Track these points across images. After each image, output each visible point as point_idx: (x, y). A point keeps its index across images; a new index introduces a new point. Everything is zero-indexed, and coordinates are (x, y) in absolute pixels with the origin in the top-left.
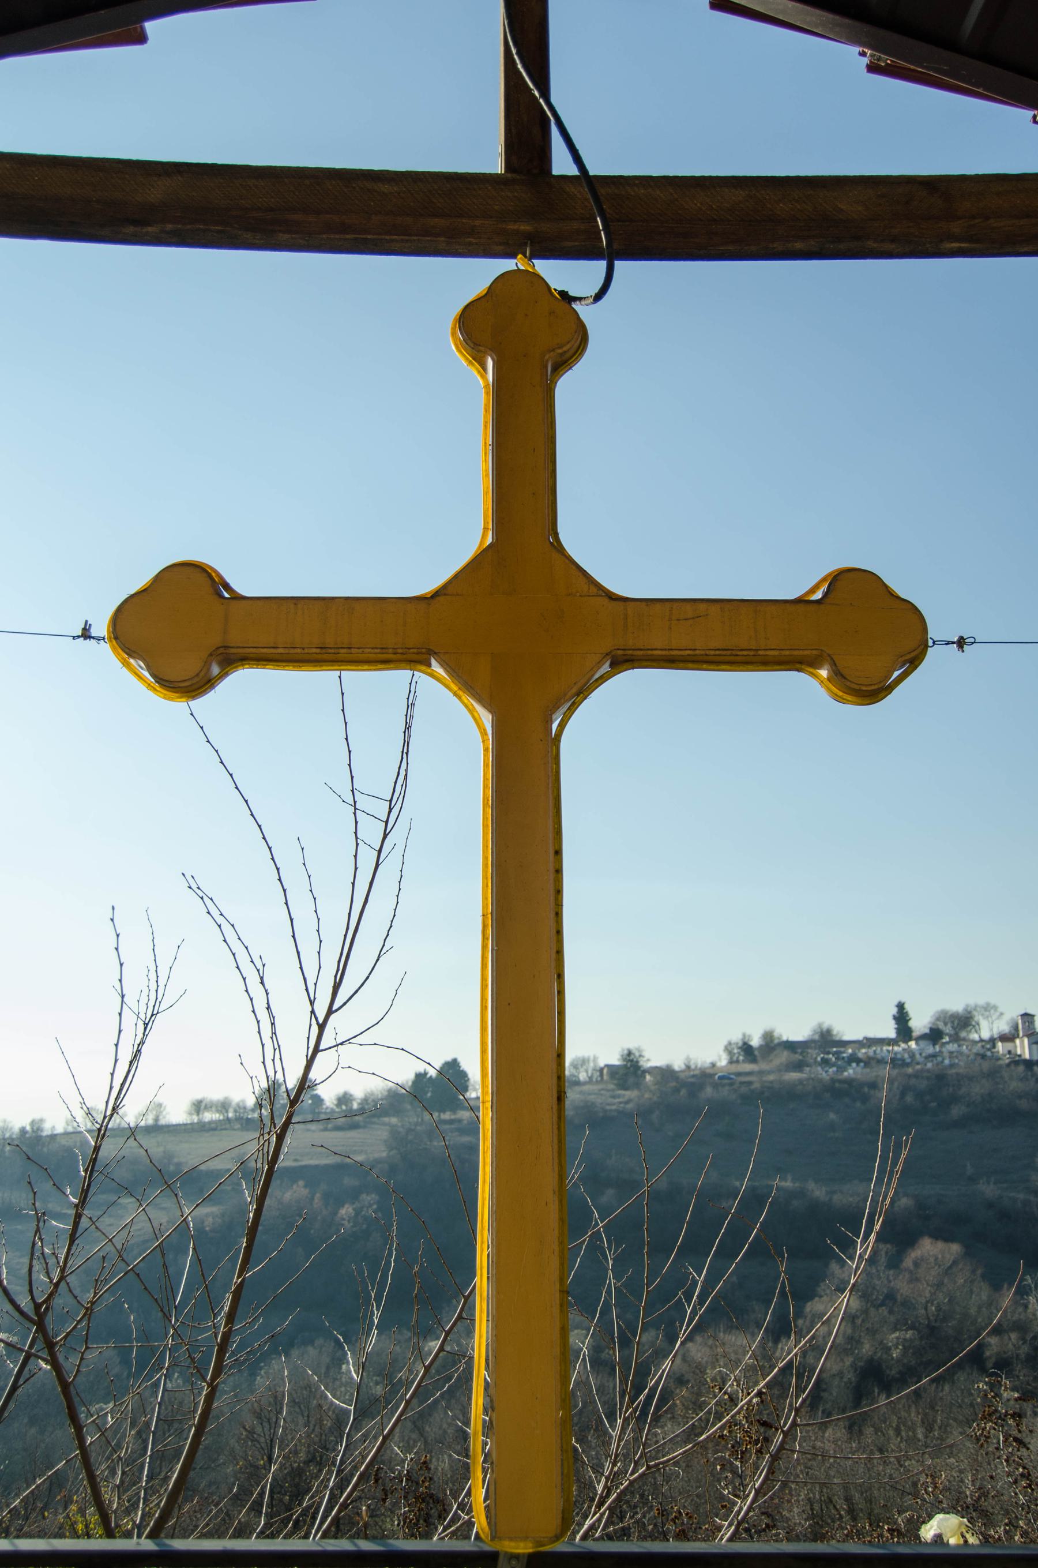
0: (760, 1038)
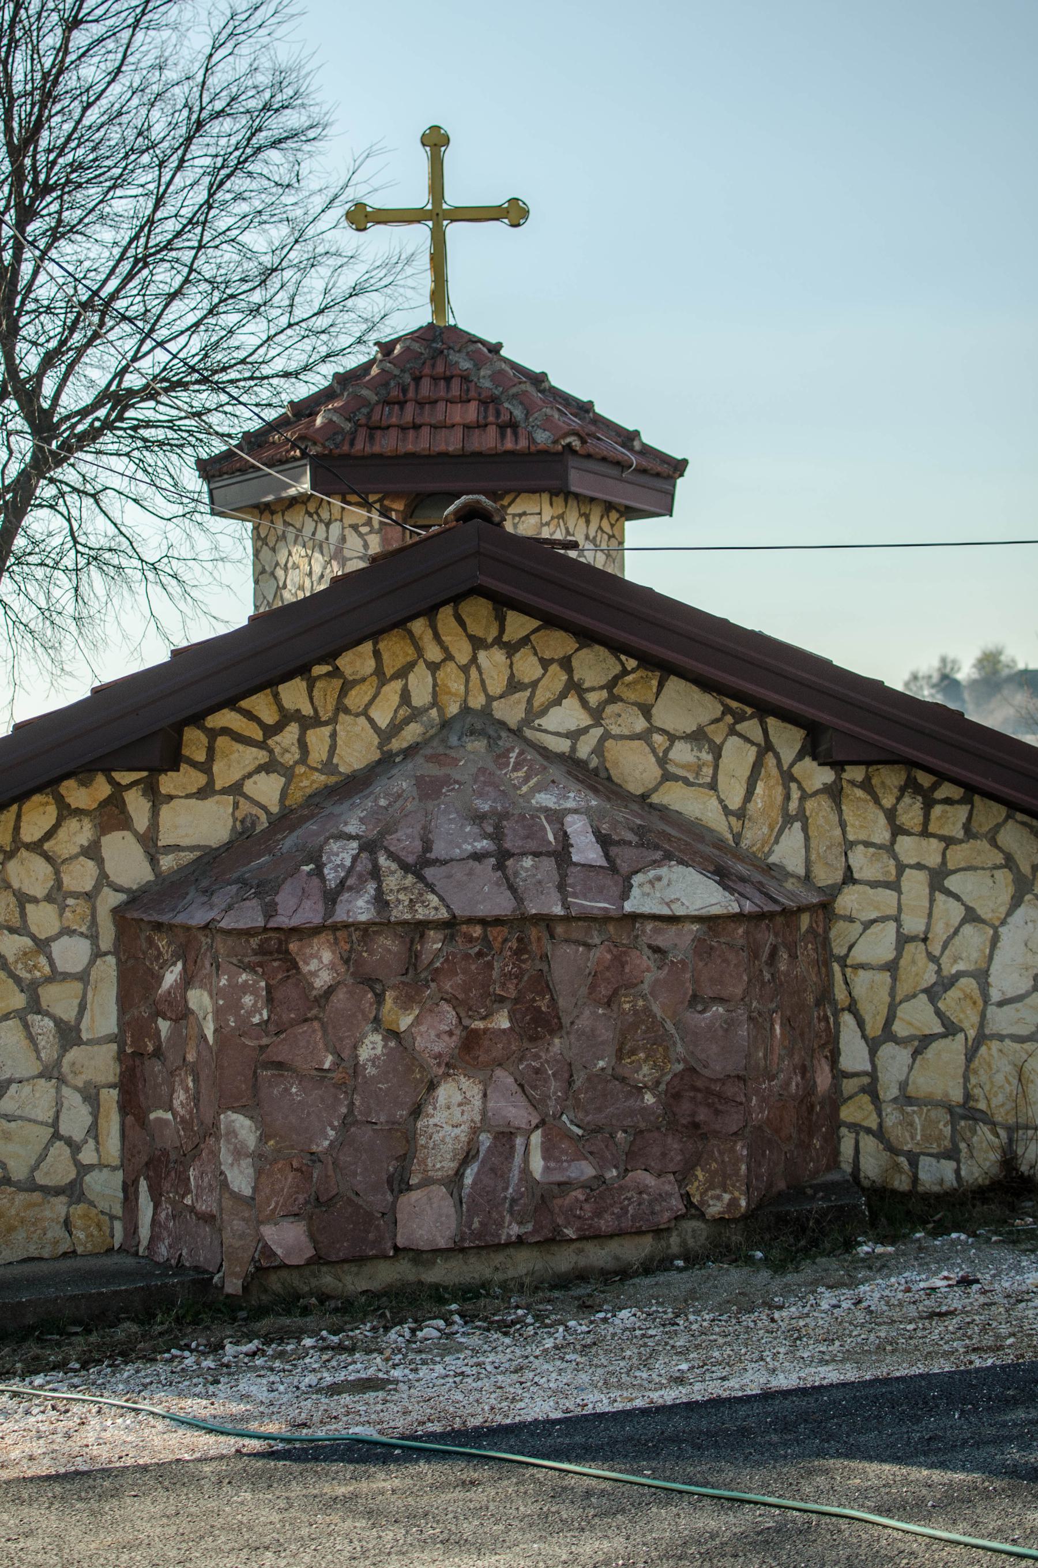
0: (974, 666)
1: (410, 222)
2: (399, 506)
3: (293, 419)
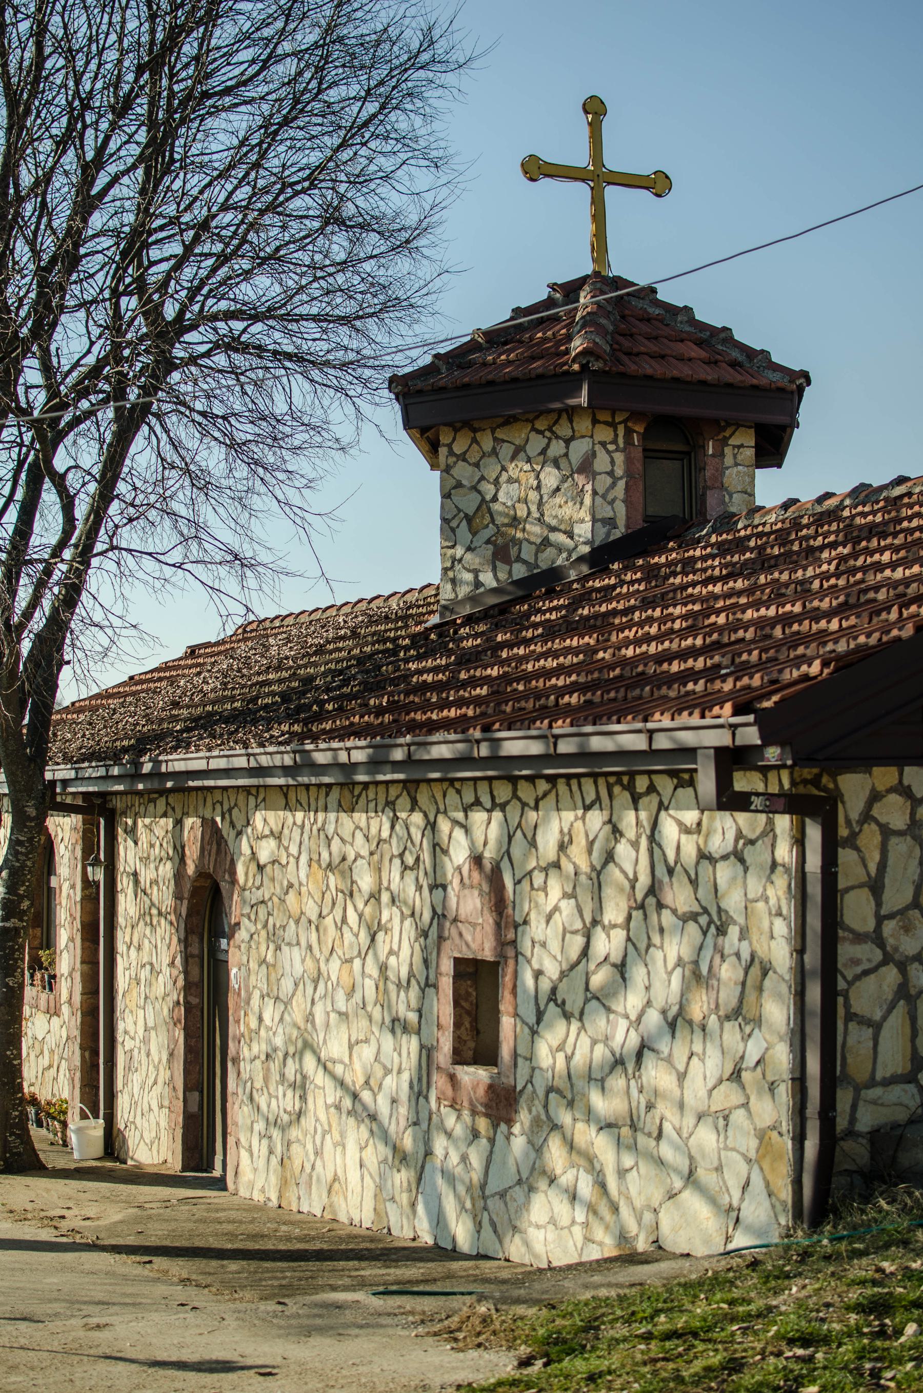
1: (576, 179)
2: (640, 428)
3: (485, 345)
